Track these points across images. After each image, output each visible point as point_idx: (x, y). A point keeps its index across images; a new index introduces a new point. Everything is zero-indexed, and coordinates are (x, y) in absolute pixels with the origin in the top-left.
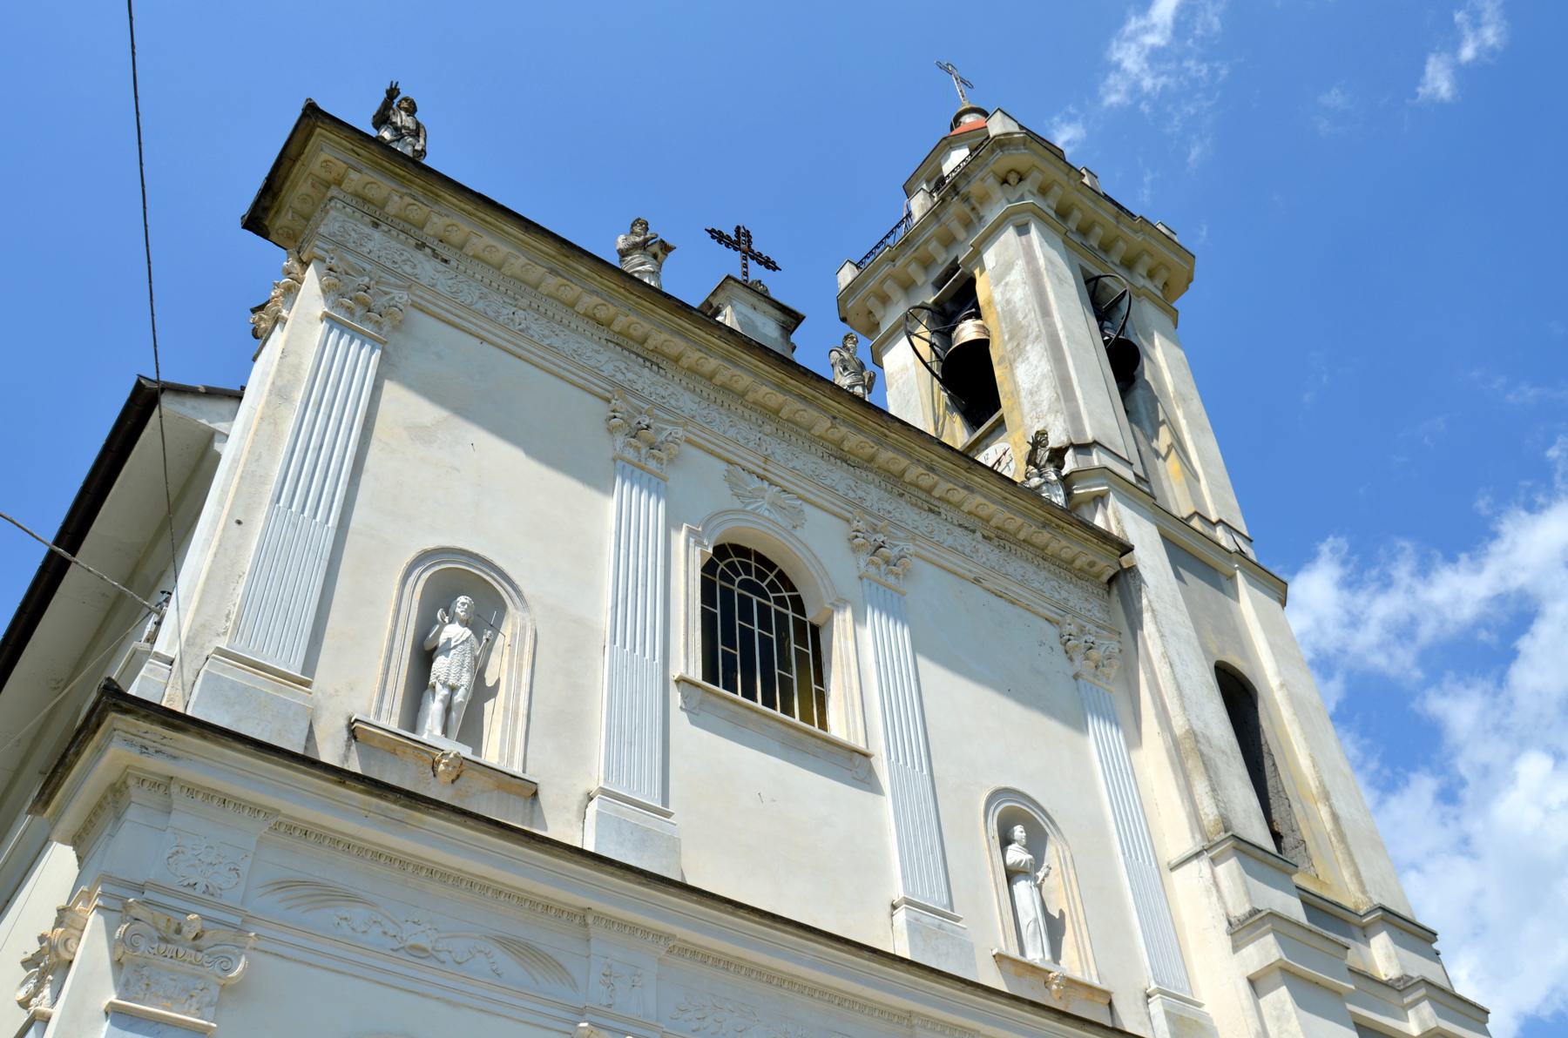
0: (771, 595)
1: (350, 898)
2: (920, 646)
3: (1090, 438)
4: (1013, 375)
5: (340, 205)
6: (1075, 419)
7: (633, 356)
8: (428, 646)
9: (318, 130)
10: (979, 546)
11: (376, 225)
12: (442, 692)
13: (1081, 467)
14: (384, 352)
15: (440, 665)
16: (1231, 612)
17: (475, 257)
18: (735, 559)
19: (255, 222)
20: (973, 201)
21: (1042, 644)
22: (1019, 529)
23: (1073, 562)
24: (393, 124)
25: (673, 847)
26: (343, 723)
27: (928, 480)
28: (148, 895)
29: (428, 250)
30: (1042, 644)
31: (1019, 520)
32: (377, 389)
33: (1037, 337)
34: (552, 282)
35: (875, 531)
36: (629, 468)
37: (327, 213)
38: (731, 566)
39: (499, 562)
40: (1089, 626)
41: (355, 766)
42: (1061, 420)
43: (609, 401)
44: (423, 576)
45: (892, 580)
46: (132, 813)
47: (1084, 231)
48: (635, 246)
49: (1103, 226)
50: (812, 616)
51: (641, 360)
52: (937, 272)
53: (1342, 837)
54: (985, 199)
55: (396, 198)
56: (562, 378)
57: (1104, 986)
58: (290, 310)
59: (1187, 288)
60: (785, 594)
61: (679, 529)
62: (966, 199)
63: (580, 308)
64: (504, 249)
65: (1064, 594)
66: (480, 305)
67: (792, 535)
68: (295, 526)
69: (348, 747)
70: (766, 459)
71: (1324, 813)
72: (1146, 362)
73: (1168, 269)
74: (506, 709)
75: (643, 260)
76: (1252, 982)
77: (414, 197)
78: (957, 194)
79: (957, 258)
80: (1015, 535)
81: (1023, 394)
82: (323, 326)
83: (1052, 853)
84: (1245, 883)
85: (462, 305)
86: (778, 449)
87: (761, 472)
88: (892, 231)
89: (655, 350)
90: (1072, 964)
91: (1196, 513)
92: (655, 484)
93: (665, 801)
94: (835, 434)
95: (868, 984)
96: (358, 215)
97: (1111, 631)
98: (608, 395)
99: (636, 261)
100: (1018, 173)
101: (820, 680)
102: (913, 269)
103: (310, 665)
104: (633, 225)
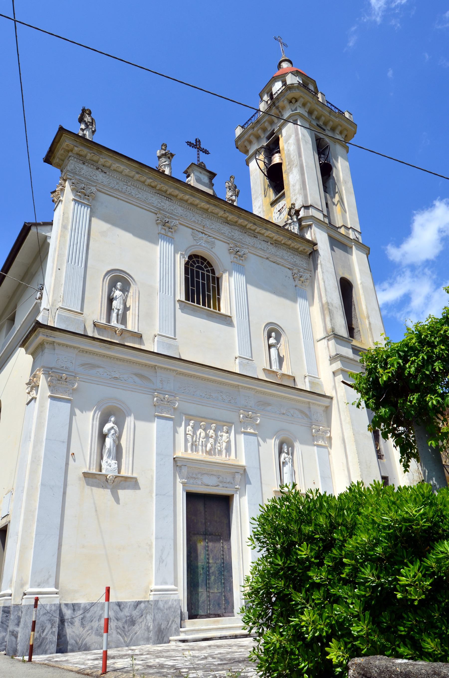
0: (205, 269)
1: (99, 367)
2: (248, 282)
3: (309, 204)
4: (288, 178)
5: (73, 159)
6: (305, 196)
7: (163, 197)
8: (111, 298)
9: (64, 135)
10: (269, 247)
11: (84, 164)
12: (116, 311)
13: (306, 215)
14: (91, 208)
15: (115, 303)
16: (349, 260)
17: (114, 170)
18: (195, 259)
19: (48, 160)
20: (280, 109)
21: (286, 276)
22: (282, 240)
23: (298, 249)
24: (85, 121)
25: (177, 347)
26: (92, 322)
27: (254, 227)
28: (53, 370)
29: (100, 170)
30: (286, 276)
31: (282, 238)
32: (90, 221)
33: (296, 166)
34: (137, 176)
35: (236, 246)
36: (163, 236)
37: (69, 161)
38: (193, 262)
39: (128, 272)
40: (302, 270)
41: (97, 336)
42: (301, 197)
43: (156, 214)
44: (108, 278)
45: (241, 262)
46: (46, 350)
47: (318, 118)
48: (163, 155)
49: (324, 116)
50: (217, 275)
51: (165, 198)
52: (268, 133)
53: (371, 329)
54: (284, 108)
55: (89, 155)
56: (142, 208)
57: (293, 375)
58: (63, 197)
59: (354, 136)
60: (209, 269)
61: (178, 253)
62: (277, 108)
63: (146, 183)
64: (122, 167)
65: (295, 260)
66: (117, 187)
67: (211, 251)
68: (74, 269)
69: (94, 329)
70: (204, 227)
71: (367, 322)
72: (334, 169)
73: (347, 130)
74: (132, 314)
75: (165, 160)
76: (334, 373)
77: (94, 153)
78: (275, 106)
79: (274, 130)
80: (281, 242)
81: (291, 185)
82: (73, 203)
83: (282, 340)
84: (335, 346)
85: (112, 188)
86: (208, 223)
87: (202, 231)
88: (254, 115)
89: (170, 194)
90: (285, 370)
91: (343, 225)
92: (170, 240)
93: (175, 336)
94: (225, 215)
95: (227, 379)
96: (78, 161)
97: (308, 270)
98: (156, 212)
99: (163, 161)
100: (295, 99)
101: (219, 294)
102: (260, 132)
103: (82, 309)
104: (162, 146)
